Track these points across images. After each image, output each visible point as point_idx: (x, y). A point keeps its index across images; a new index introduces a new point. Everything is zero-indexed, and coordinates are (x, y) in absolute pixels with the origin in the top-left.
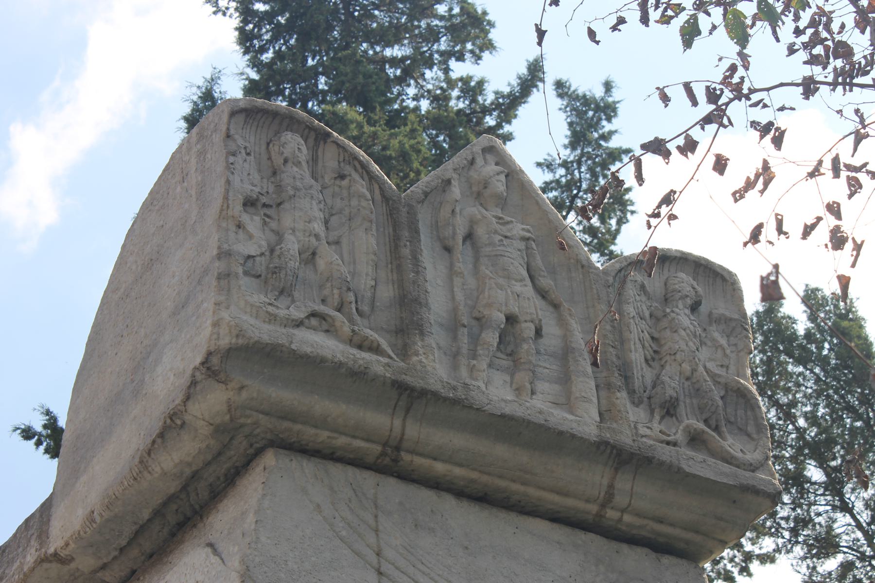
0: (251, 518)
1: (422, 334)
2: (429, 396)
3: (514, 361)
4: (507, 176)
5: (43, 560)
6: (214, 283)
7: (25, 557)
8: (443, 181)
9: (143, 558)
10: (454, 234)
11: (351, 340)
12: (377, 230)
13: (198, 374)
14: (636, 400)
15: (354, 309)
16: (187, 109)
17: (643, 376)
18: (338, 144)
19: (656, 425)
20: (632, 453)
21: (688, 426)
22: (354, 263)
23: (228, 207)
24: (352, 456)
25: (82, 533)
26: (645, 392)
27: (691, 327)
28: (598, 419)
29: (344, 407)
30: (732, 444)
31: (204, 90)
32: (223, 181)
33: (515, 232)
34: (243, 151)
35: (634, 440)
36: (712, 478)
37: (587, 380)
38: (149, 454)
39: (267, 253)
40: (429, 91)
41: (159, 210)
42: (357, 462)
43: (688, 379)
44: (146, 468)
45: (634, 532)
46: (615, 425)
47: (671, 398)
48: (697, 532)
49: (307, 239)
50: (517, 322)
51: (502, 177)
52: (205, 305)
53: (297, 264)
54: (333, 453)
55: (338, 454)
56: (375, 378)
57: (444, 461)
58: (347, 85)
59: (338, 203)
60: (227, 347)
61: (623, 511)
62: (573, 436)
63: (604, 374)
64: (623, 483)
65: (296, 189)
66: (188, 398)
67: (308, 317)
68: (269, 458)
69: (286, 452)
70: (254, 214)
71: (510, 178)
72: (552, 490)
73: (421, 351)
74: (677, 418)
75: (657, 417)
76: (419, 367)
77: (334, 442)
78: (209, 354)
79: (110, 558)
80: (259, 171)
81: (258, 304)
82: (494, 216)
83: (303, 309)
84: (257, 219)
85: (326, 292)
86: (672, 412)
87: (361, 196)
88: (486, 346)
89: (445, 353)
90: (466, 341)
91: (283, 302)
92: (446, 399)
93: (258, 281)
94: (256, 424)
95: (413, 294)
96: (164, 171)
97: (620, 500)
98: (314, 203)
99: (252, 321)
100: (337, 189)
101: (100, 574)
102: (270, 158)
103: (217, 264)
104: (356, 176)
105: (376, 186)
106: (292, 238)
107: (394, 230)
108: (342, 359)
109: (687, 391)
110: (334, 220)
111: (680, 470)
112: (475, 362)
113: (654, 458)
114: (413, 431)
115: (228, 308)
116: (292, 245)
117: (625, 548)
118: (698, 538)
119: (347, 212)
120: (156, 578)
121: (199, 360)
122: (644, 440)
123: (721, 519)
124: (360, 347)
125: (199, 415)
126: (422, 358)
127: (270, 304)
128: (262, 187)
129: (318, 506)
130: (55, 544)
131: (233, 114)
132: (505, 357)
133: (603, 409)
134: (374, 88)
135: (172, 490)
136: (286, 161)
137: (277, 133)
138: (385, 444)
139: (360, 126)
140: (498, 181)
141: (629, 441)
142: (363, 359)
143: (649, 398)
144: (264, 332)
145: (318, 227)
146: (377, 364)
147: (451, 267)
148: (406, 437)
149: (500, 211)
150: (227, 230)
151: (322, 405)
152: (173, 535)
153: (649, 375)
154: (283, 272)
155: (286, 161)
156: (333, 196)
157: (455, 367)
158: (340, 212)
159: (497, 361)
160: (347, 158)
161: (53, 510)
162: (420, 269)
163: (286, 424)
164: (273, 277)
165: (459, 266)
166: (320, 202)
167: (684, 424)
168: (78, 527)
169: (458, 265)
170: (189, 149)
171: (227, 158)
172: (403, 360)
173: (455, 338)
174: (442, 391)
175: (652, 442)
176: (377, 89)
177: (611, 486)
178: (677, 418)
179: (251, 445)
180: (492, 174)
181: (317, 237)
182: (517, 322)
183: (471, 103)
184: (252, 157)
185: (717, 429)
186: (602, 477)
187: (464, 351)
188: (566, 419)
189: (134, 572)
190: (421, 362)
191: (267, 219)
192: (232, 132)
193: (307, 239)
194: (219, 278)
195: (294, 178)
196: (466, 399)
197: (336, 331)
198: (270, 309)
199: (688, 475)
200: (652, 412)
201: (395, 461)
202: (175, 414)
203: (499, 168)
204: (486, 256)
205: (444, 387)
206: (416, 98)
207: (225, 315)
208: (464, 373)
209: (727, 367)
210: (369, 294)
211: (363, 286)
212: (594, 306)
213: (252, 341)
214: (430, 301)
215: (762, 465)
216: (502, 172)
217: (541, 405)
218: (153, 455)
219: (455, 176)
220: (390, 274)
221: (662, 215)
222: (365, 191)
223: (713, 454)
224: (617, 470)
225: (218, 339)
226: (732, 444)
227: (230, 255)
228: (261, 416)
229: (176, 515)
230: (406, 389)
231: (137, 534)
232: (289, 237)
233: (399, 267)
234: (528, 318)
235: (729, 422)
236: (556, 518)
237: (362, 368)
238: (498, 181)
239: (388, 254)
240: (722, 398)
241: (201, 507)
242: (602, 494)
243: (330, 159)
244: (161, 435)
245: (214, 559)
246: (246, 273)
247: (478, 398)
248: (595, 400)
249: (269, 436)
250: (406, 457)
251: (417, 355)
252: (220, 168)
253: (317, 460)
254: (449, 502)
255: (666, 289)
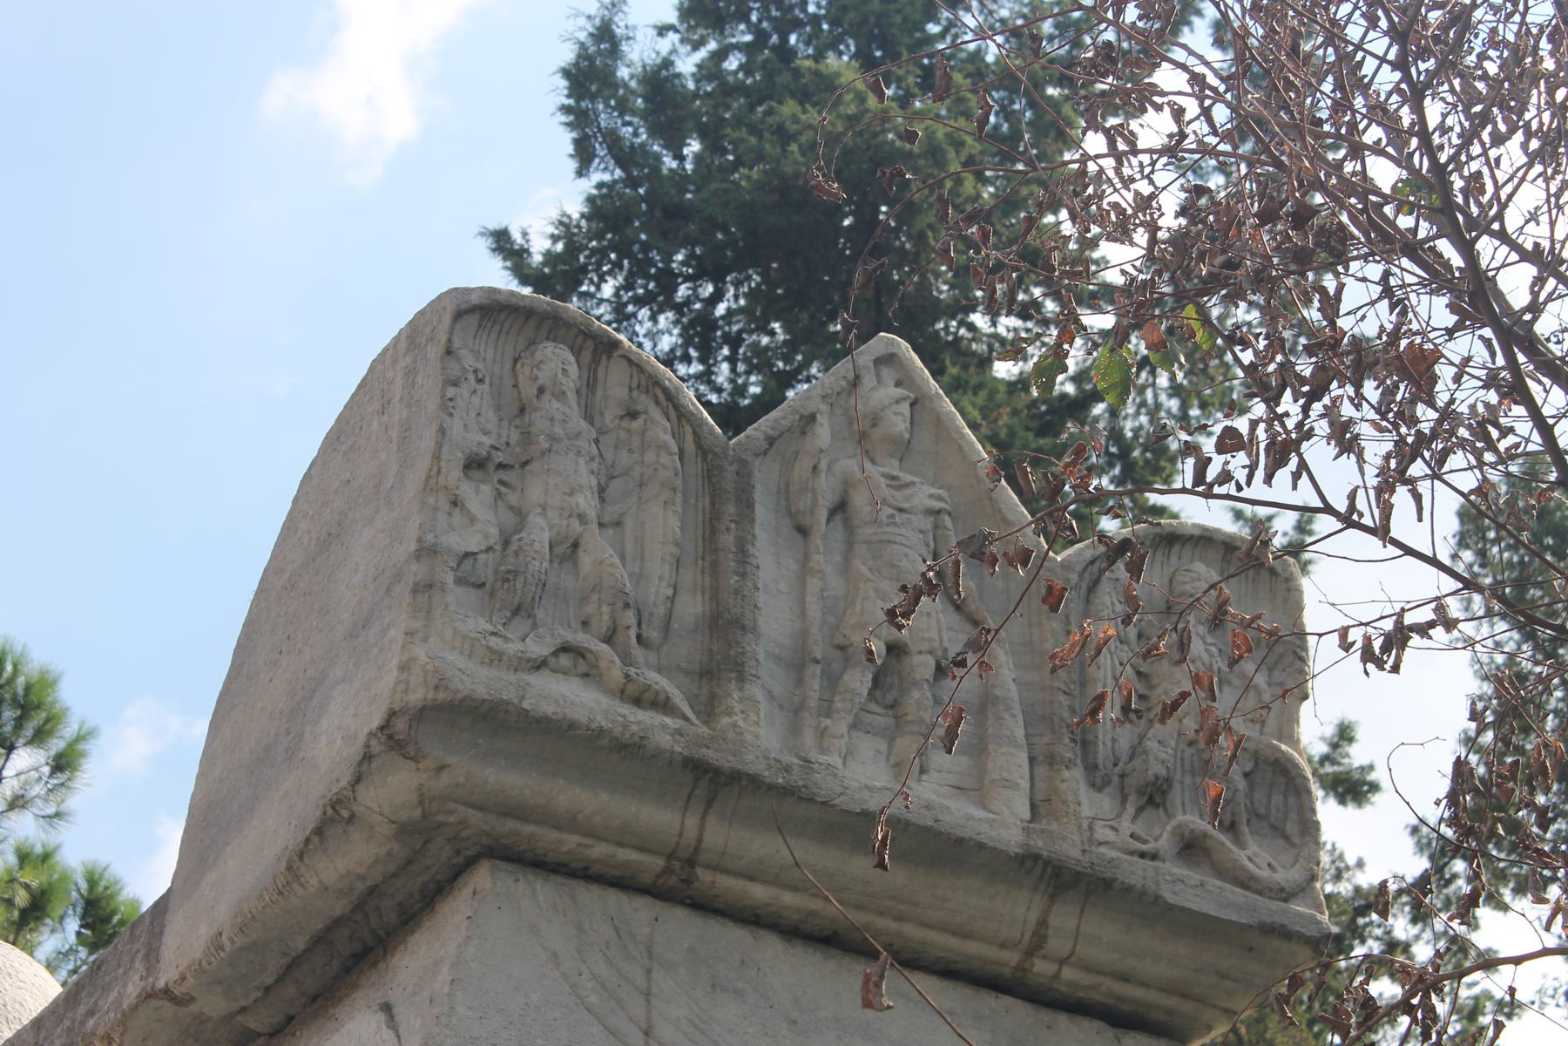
0: (445, 974)
1: (741, 678)
2: (744, 782)
3: (896, 717)
4: (912, 405)
5: (148, 995)
6: (407, 598)
7: (125, 985)
8: (802, 417)
9: (303, 1000)
10: (814, 503)
11: (623, 691)
12: (685, 501)
13: (374, 743)
14: (1098, 781)
15: (634, 640)
16: (567, 55)
17: (1114, 740)
18: (630, 361)
19: (1126, 826)
20: (1078, 873)
21: (1179, 826)
22: (642, 558)
23: (439, 471)
24: (616, 873)
25: (204, 964)
26: (1115, 765)
27: (1205, 657)
28: (1027, 815)
29: (605, 797)
30: (1255, 856)
31: (597, 22)
32: (435, 427)
33: (916, 501)
34: (472, 377)
35: (1084, 851)
36: (1212, 913)
37: (1014, 751)
38: (301, 857)
39: (498, 547)
40: (1002, 21)
41: (346, 453)
42: (624, 883)
43: (1191, 743)
44: (297, 878)
45: (1080, 994)
46: (1054, 826)
47: (1157, 778)
48: (1185, 996)
49: (565, 523)
50: (906, 653)
51: (905, 408)
52: (393, 632)
53: (545, 564)
54: (586, 868)
55: (596, 869)
56: (657, 753)
57: (766, 882)
58: (852, 15)
59: (624, 458)
60: (420, 704)
61: (1062, 962)
62: (981, 846)
63: (1046, 739)
64: (1064, 918)
65: (553, 439)
66: (358, 779)
67: (555, 653)
68: (482, 877)
69: (510, 866)
70: (482, 481)
71: (917, 407)
72: (944, 929)
73: (737, 707)
74: (1166, 810)
75: (1131, 810)
76: (731, 735)
77: (587, 852)
78: (392, 714)
79: (251, 1000)
80: (498, 408)
81: (473, 635)
82: (883, 475)
83: (549, 640)
84: (486, 489)
85: (590, 609)
86: (1158, 799)
87: (662, 447)
88: (848, 696)
89: (781, 707)
90: (816, 687)
91: (520, 626)
92: (771, 787)
93: (479, 592)
94: (463, 823)
95: (734, 611)
96: (360, 387)
97: (1057, 945)
98: (581, 461)
99: (462, 662)
100: (623, 435)
101: (240, 1018)
102: (515, 386)
103: (414, 567)
104: (655, 413)
105: (688, 429)
106: (540, 521)
107: (713, 504)
108: (603, 723)
109: (1187, 763)
110: (615, 487)
111: (1157, 899)
112: (828, 722)
113: (1115, 880)
114: (718, 835)
115: (425, 640)
116: (539, 534)
117: (1062, 1019)
118: (1186, 1007)
119: (637, 470)
120: (315, 1040)
121: (376, 721)
122: (1103, 849)
123: (1225, 976)
124: (637, 702)
125: (374, 806)
126: (738, 719)
127: (494, 634)
128: (500, 436)
129: (555, 955)
130: (166, 976)
131: (459, 315)
132: (881, 711)
133: (1039, 796)
134: (898, 19)
135: (338, 912)
136: (541, 391)
137: (532, 343)
138: (671, 856)
139: (860, 98)
140: (896, 414)
141: (1075, 853)
142: (639, 723)
143: (1122, 776)
144: (479, 681)
145: (586, 502)
146: (659, 730)
147: (805, 561)
148: (704, 845)
149: (896, 463)
150: (436, 509)
151: (570, 795)
152: (347, 970)
153: (1126, 736)
154: (521, 579)
155: (541, 391)
156: (616, 447)
157: (795, 729)
158: (627, 472)
159: (868, 718)
160: (643, 383)
161: (168, 917)
162: (749, 568)
163: (511, 824)
164: (505, 587)
165: (817, 559)
166: (592, 459)
167: (1174, 822)
168: (198, 955)
169: (815, 557)
170: (395, 361)
171: (443, 389)
172: (706, 723)
173: (800, 682)
174: (766, 773)
175: (1114, 854)
176: (905, 20)
177: (1043, 923)
178: (1166, 810)
179: (458, 852)
180: (886, 403)
181: (582, 518)
182: (906, 653)
183: (1072, 48)
184: (486, 386)
185: (1231, 828)
186: (1029, 909)
187: (813, 704)
188: (969, 818)
189: (290, 1019)
190: (734, 725)
191: (502, 489)
192: (456, 344)
193: (565, 523)
194: (415, 591)
195: (552, 420)
196: (805, 786)
197: (601, 675)
198: (494, 642)
199: (1171, 908)
200: (1124, 799)
201: (687, 882)
202: (339, 801)
203: (900, 392)
204: (865, 542)
205: (769, 767)
206: (981, 34)
207: (420, 652)
208: (809, 739)
209: (1263, 723)
210: (661, 611)
211: (652, 598)
212: (1040, 624)
213: (460, 696)
214: (761, 623)
215: (1303, 890)
216: (904, 399)
217: (937, 795)
218: (306, 860)
219: (824, 407)
220: (699, 576)
221: (969, 664)
222: (668, 438)
223: (1221, 872)
224: (1053, 898)
225: (406, 691)
226: (1255, 856)
227: (435, 552)
228: (471, 811)
229: (351, 945)
230: (706, 772)
231: (289, 968)
232: (535, 520)
233: (715, 566)
234: (925, 647)
235: (1258, 816)
236: (949, 972)
237: (636, 738)
238: (896, 414)
239: (700, 543)
240: (1246, 775)
241: (388, 934)
242: (1027, 937)
243: (615, 383)
244: (319, 831)
245: (388, 1035)
246: (459, 581)
247: (824, 785)
248: (1025, 784)
249: (485, 841)
250: (704, 876)
251: (729, 715)
252: (432, 404)
253: (560, 879)
254: (772, 948)
255: (1171, 591)
